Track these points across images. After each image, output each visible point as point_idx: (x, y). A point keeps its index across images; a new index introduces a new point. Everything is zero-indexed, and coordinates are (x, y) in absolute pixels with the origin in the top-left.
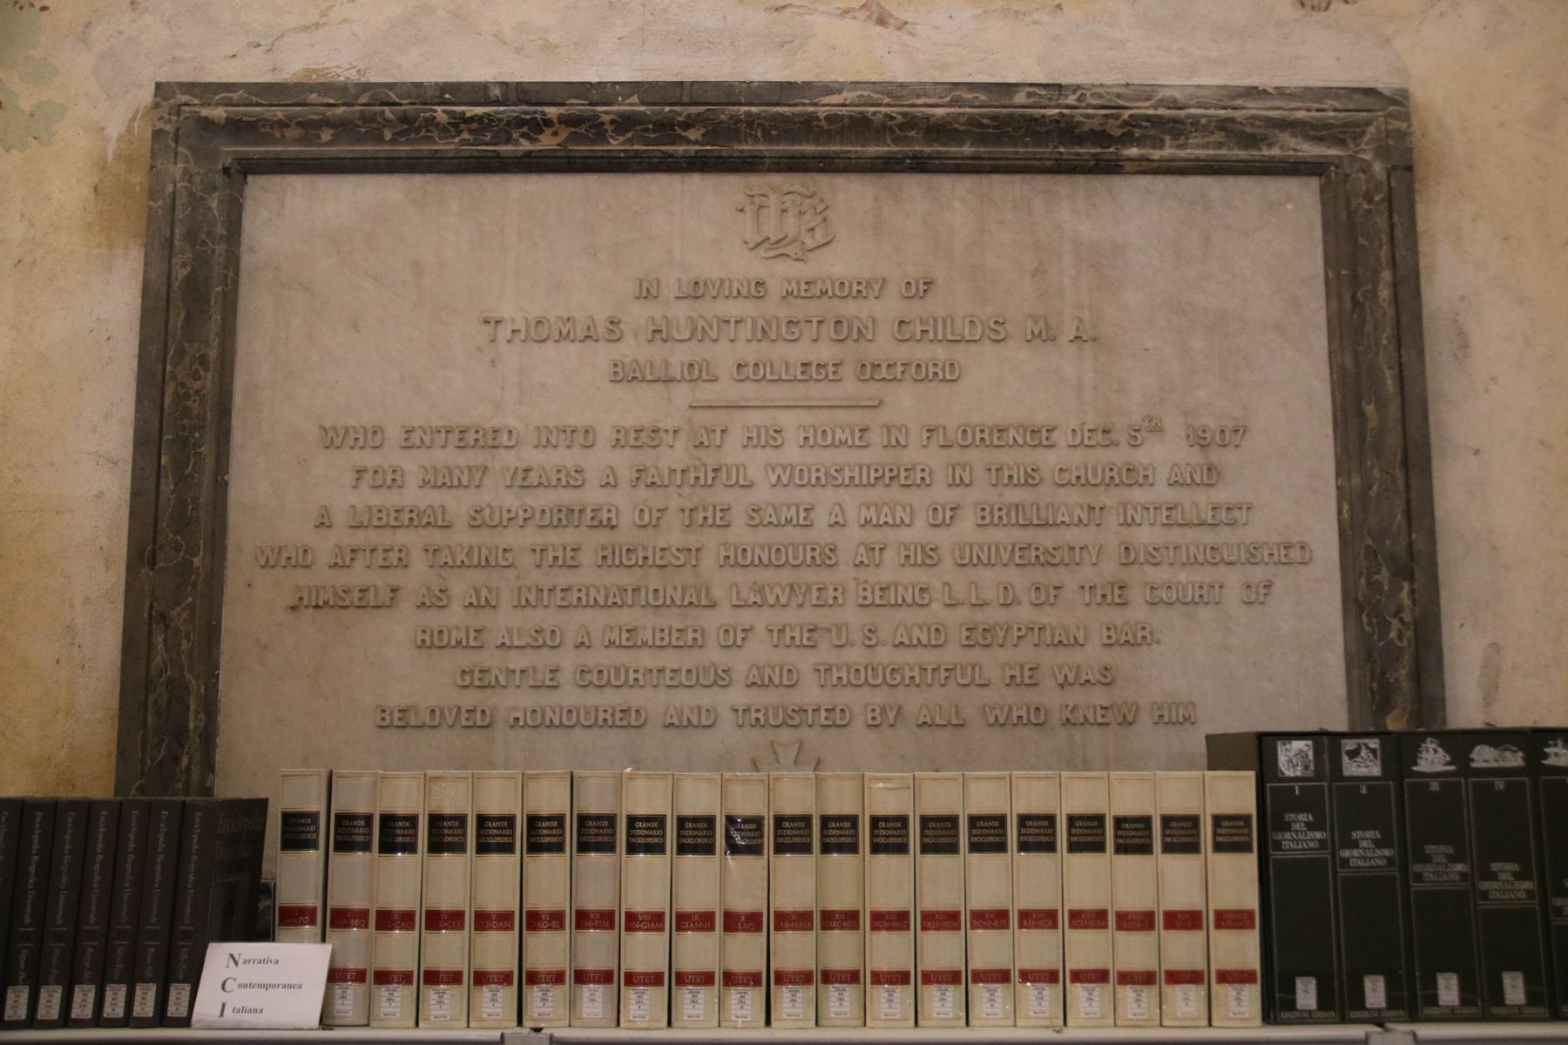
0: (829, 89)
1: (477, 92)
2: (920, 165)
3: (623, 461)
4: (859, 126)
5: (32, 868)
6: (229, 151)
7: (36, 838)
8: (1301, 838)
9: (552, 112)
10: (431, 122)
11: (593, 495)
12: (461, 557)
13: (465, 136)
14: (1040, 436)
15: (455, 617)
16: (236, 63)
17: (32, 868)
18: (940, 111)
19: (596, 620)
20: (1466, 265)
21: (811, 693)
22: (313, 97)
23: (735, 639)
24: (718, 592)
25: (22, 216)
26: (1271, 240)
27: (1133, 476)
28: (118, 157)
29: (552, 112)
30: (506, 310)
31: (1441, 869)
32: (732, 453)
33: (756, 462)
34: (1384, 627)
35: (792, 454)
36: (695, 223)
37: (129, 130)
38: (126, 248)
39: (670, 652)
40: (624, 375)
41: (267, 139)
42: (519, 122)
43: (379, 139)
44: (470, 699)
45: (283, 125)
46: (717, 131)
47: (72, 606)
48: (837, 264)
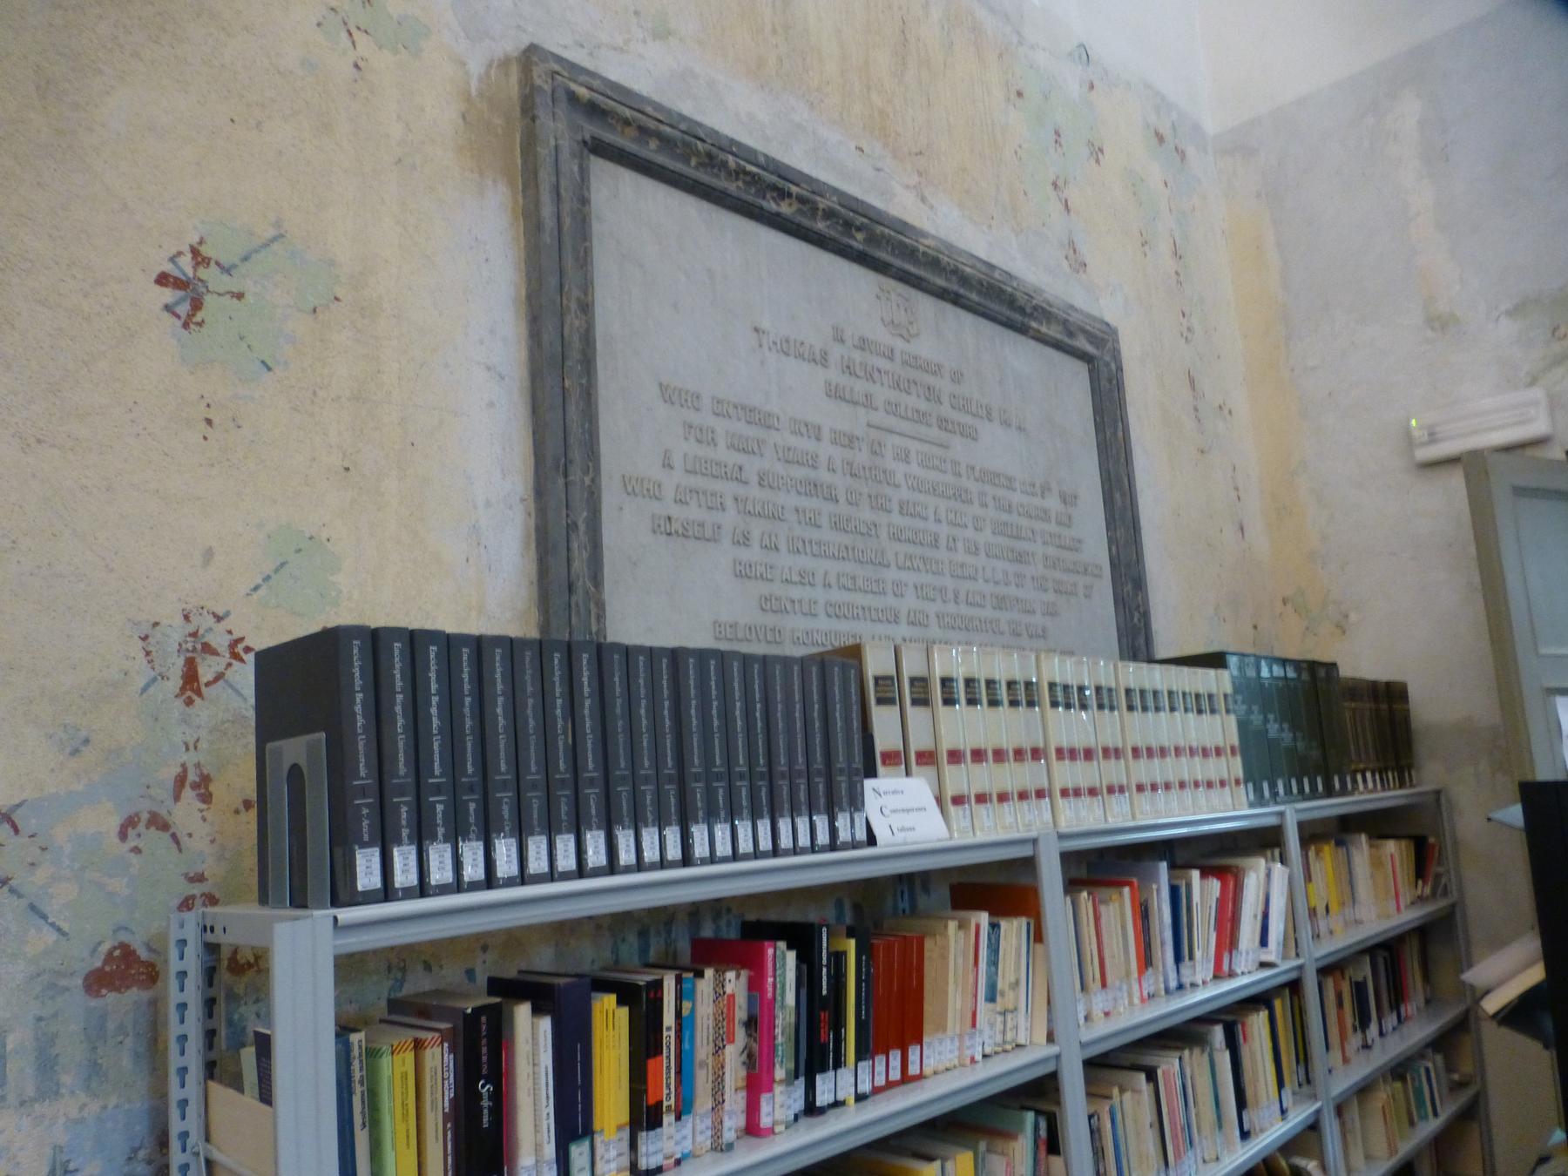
0: (924, 235)
2: (956, 300)
3: (838, 454)
4: (935, 264)
5: (434, 711)
6: (591, 129)
7: (433, 676)
9: (794, 189)
10: (724, 164)
11: (824, 476)
12: (758, 508)
13: (740, 183)
14: (1009, 483)
15: (754, 554)
17: (434, 711)
18: (968, 270)
19: (833, 567)
22: (649, 110)
23: (898, 590)
24: (890, 557)
25: (399, 117)
28: (481, 95)
29: (794, 189)
30: (765, 324)
32: (889, 463)
33: (900, 469)
34: (1132, 617)
35: (915, 469)
36: (855, 293)
37: (487, 74)
38: (494, 181)
39: (870, 596)
40: (835, 393)
41: (612, 128)
42: (774, 188)
43: (687, 161)
44: (770, 620)
45: (627, 122)
46: (872, 239)
47: (475, 507)
48: (925, 348)
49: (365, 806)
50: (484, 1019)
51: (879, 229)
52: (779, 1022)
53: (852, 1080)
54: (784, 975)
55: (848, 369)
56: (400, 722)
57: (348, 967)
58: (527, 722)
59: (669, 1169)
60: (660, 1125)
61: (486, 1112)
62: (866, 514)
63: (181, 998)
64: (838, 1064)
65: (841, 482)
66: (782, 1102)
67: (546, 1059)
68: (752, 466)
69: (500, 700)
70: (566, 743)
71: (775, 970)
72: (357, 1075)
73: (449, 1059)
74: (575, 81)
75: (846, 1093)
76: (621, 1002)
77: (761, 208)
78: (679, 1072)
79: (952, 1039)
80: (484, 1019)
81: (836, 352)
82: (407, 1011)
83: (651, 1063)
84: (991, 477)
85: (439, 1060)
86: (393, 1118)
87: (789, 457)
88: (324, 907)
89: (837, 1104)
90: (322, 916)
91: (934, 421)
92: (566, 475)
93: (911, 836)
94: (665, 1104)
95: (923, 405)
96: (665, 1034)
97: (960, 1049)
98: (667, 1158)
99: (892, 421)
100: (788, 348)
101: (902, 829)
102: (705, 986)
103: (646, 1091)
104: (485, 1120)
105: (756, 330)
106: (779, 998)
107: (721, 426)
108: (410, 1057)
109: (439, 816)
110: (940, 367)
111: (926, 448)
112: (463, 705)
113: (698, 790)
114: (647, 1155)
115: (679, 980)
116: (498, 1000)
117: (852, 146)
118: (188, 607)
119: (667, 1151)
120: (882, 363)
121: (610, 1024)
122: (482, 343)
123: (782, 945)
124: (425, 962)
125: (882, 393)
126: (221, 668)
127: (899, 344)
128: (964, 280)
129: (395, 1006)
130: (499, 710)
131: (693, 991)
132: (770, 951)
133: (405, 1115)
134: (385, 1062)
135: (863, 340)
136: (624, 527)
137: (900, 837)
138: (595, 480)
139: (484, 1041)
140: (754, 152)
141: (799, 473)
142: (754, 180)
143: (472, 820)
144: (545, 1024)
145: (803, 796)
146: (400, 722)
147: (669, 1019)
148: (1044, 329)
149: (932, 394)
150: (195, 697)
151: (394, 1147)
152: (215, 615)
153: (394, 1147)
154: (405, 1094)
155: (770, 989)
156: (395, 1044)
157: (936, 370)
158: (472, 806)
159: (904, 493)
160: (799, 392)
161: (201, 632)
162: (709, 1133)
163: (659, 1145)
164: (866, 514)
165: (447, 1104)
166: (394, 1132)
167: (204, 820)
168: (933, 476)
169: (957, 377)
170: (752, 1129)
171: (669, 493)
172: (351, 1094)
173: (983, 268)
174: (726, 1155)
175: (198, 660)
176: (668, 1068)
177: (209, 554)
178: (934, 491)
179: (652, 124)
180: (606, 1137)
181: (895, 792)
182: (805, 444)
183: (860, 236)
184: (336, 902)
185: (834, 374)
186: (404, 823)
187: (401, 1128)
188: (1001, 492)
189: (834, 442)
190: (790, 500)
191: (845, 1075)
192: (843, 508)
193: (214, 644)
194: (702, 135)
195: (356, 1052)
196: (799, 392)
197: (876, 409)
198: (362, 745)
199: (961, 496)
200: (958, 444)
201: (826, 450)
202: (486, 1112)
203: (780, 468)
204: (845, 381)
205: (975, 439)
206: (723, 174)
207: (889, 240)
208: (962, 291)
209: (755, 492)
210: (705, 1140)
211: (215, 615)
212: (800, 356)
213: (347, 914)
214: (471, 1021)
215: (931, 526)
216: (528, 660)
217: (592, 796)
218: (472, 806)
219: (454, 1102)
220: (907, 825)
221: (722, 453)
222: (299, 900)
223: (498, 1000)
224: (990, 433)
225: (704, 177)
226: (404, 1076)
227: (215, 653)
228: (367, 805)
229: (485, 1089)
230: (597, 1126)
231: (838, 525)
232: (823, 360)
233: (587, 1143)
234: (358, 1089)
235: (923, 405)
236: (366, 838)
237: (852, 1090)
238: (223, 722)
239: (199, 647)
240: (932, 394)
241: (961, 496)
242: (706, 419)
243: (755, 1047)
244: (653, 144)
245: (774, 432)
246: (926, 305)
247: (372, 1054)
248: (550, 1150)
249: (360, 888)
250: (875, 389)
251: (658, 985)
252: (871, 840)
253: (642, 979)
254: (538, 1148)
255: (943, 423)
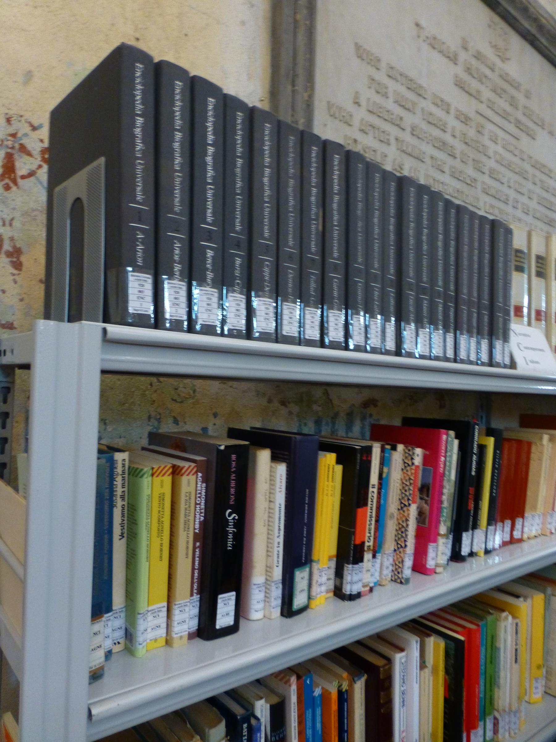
3: (459, 126)
40: (460, 85)
48: (512, 69)
49: (141, 230)
50: (234, 457)
52: (445, 491)
53: (484, 539)
54: (451, 456)
55: (468, 70)
56: (178, 160)
57: (121, 391)
58: (287, 202)
59: (366, 595)
60: (361, 560)
61: (230, 536)
62: (470, 171)
63: (278, 549)
64: (475, 526)
65: (459, 146)
66: (439, 551)
67: (280, 498)
68: (409, 119)
69: (267, 171)
70: (317, 229)
72: (119, 490)
73: (202, 487)
75: (479, 547)
76: (339, 461)
78: (377, 521)
79: (539, 516)
80: (234, 457)
81: (463, 56)
82: (166, 444)
83: (360, 511)
84: (539, 166)
85: (193, 486)
86: (149, 531)
88: (97, 321)
89: (472, 554)
90: (91, 329)
91: (512, 120)
92: (293, 86)
94: (367, 544)
95: (509, 109)
96: (371, 490)
97: (543, 523)
98: (364, 586)
99: (489, 113)
100: (434, 43)
101: (532, 362)
102: (398, 455)
103: (354, 533)
104: (230, 543)
105: (417, 25)
106: (447, 473)
107: (392, 86)
108: (168, 480)
109: (209, 261)
110: (519, 84)
111: (507, 137)
112: (235, 166)
113: (411, 296)
114: (352, 583)
115: (383, 450)
116: (247, 443)
118: (11, 112)
119: (365, 581)
120: (488, 72)
121: (329, 474)
123: (452, 433)
124: (174, 418)
125: (487, 94)
126: (34, 167)
127: (498, 61)
129: (156, 438)
130: (266, 180)
131: (390, 460)
132: (444, 437)
133: (160, 531)
134: (146, 481)
135: (479, 53)
138: (311, 96)
139: (233, 476)
141: (436, 132)
143: (237, 273)
144: (282, 469)
145: (475, 324)
146: (178, 160)
147: (374, 479)
149: (513, 103)
150: (11, 185)
151: (148, 559)
152: (31, 125)
153: (148, 559)
154: (161, 513)
155: (442, 466)
156: (156, 467)
157: (517, 87)
158: (238, 261)
159: (492, 164)
160: (438, 76)
161: (19, 135)
162: (391, 568)
163: (360, 576)
164: (470, 171)
165: (197, 526)
166: (149, 546)
167: (15, 282)
168: (508, 156)
169: (528, 96)
170: (419, 567)
171: (356, 122)
172: (112, 506)
174: (403, 587)
175: (16, 156)
176: (371, 517)
177: (29, 76)
178: (508, 167)
180: (320, 566)
181: (525, 335)
182: (439, 113)
184: (106, 319)
185: (459, 70)
186: (176, 258)
187: (156, 542)
188: (544, 178)
189: (457, 118)
190: (429, 150)
191: (479, 534)
192: (457, 163)
193: (29, 147)
195: (119, 470)
196: (438, 76)
197: (482, 102)
198: (140, 168)
199: (523, 174)
200: (525, 140)
201: (452, 122)
202: (230, 536)
203: (424, 126)
204: (465, 76)
205: (534, 139)
208: (538, 36)
209: (407, 137)
210: (388, 573)
211: (31, 125)
214: (223, 456)
215: (504, 189)
216: (291, 144)
217: (336, 280)
218: (238, 261)
219: (203, 525)
220: (535, 359)
221: (390, 104)
222: (75, 316)
223: (247, 443)
224: (542, 136)
226: (162, 497)
227: (29, 154)
228: (143, 231)
229: (231, 517)
230: (315, 556)
232: (453, 59)
233: (307, 569)
234: (119, 503)
235: (509, 109)
236: (140, 262)
237: (483, 546)
238: (34, 210)
239: (17, 146)
240: (513, 103)
241: (523, 174)
242: (381, 77)
243: (426, 508)
245: (421, 99)
246: (516, 42)
247: (134, 473)
248: (278, 573)
249: (131, 310)
250: (482, 88)
251: (368, 450)
252: (513, 365)
253: (358, 444)
254: (268, 569)
255: (518, 124)
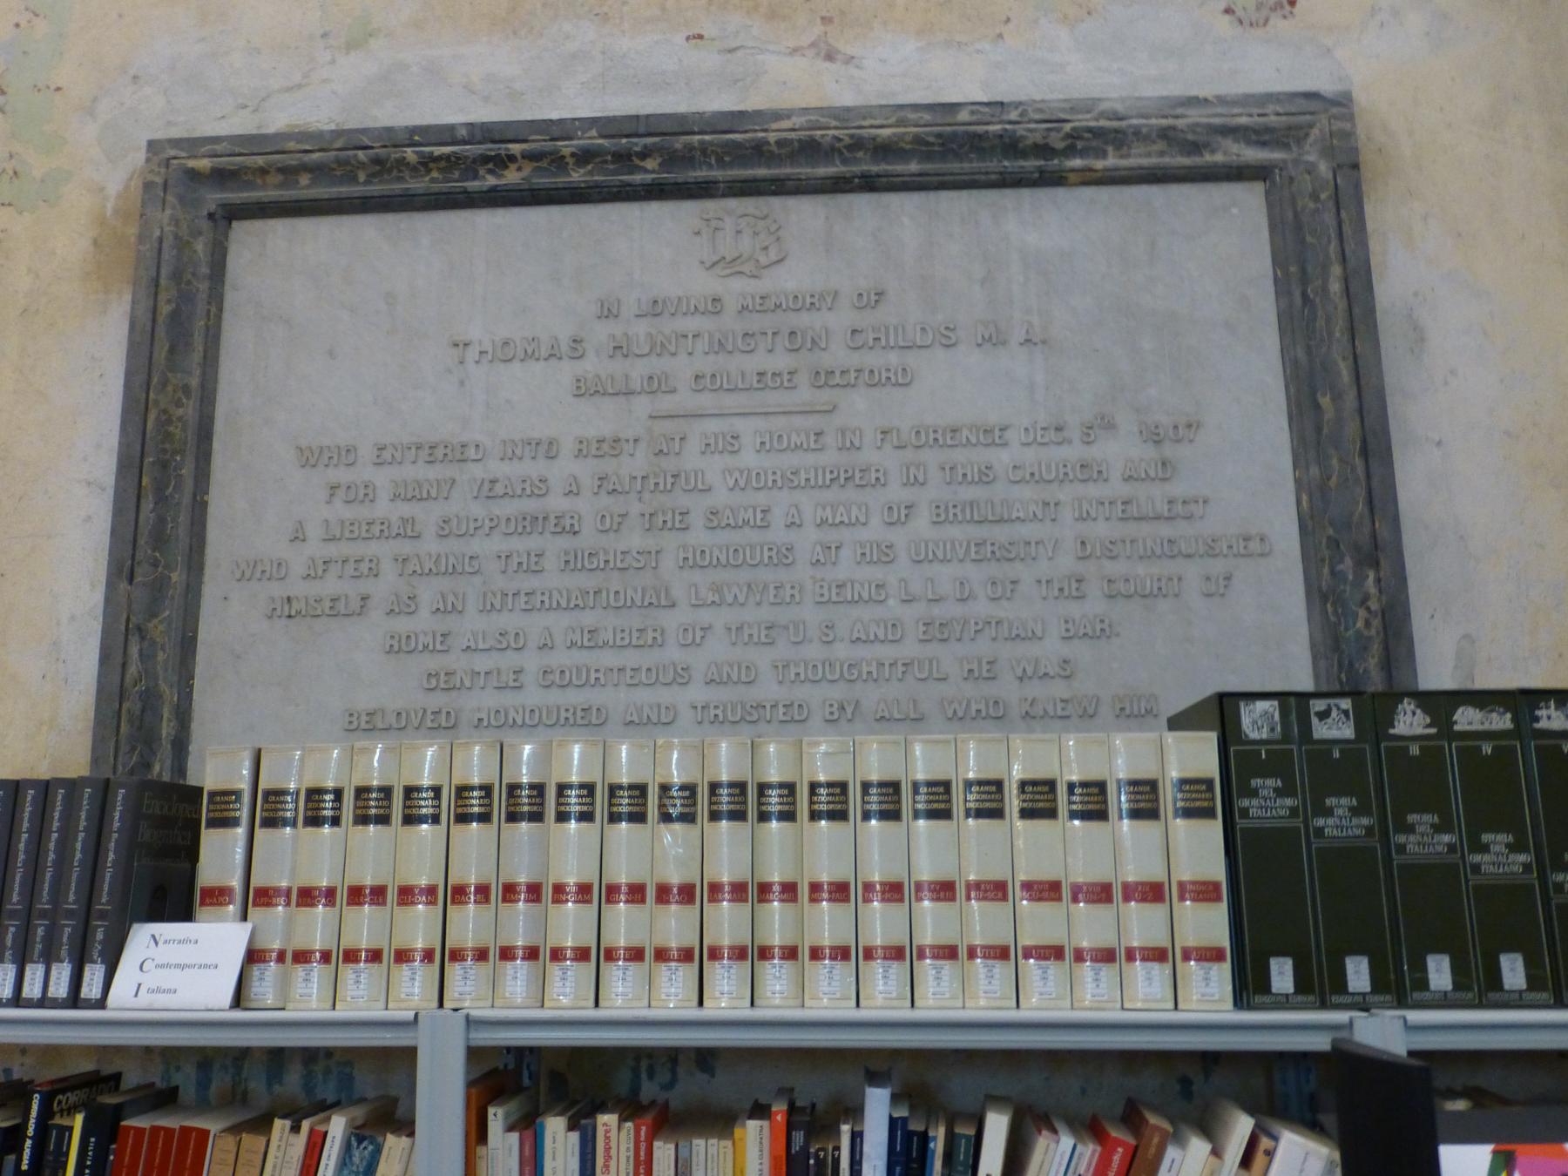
1: (446, 134)
3: (586, 471)
4: (809, 149)
6: (213, 198)
8: (1268, 804)
9: (516, 148)
10: (402, 163)
12: (428, 565)
13: (435, 174)
14: (993, 435)
16: (221, 118)
18: (886, 132)
19: (559, 622)
20: (1412, 260)
21: (769, 690)
22: (292, 145)
23: (695, 637)
26: (1220, 243)
27: (1090, 471)
29: (516, 148)
30: (475, 332)
31: (1424, 839)
36: (653, 244)
40: (585, 390)
41: (250, 186)
42: (485, 159)
43: (353, 179)
44: (438, 701)
45: (263, 171)
46: (673, 159)
47: (58, 624)
48: (791, 279)
51: (679, 143)
68: (428, 516)
71: (608, 1157)
74: (195, 157)
77: (465, 192)
87: (489, 490)
93: (162, 1000)
107: (382, 479)
117: (679, 39)
122: (85, 459)
128: (885, 150)
136: (228, 616)
137: (145, 999)
140: (451, 128)
142: (451, 162)
148: (1099, 164)
160: (537, 402)
164: (634, 539)
173: (927, 117)
179: (291, 160)
183: (650, 164)
194: (368, 142)
203: (478, 510)
206: (407, 174)
207: (704, 149)
212: (527, 356)
213: (1415, 1016)
221: (383, 508)
225: (377, 189)
231: (569, 564)
244: (304, 180)
